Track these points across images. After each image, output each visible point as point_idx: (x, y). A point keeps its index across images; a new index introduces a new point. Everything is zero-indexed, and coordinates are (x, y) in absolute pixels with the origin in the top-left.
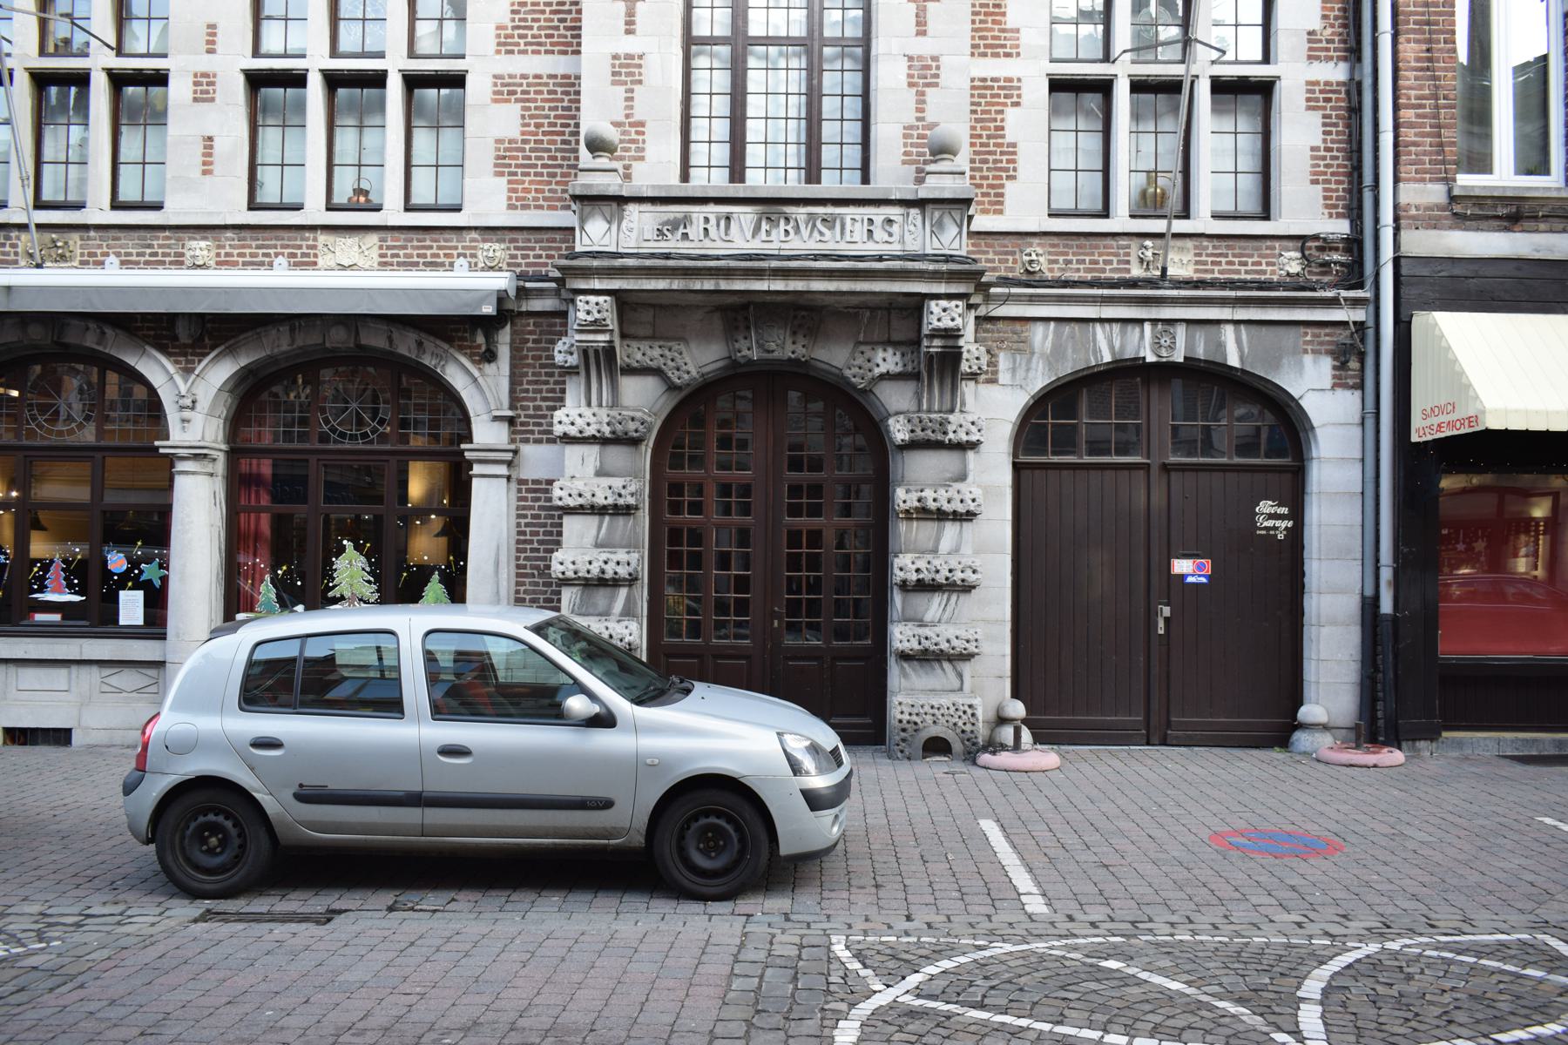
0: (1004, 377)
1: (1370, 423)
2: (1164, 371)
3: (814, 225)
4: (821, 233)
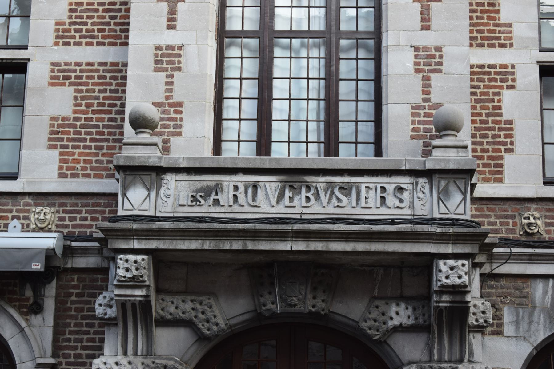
0: (508, 330)
3: (333, 193)
4: (339, 200)
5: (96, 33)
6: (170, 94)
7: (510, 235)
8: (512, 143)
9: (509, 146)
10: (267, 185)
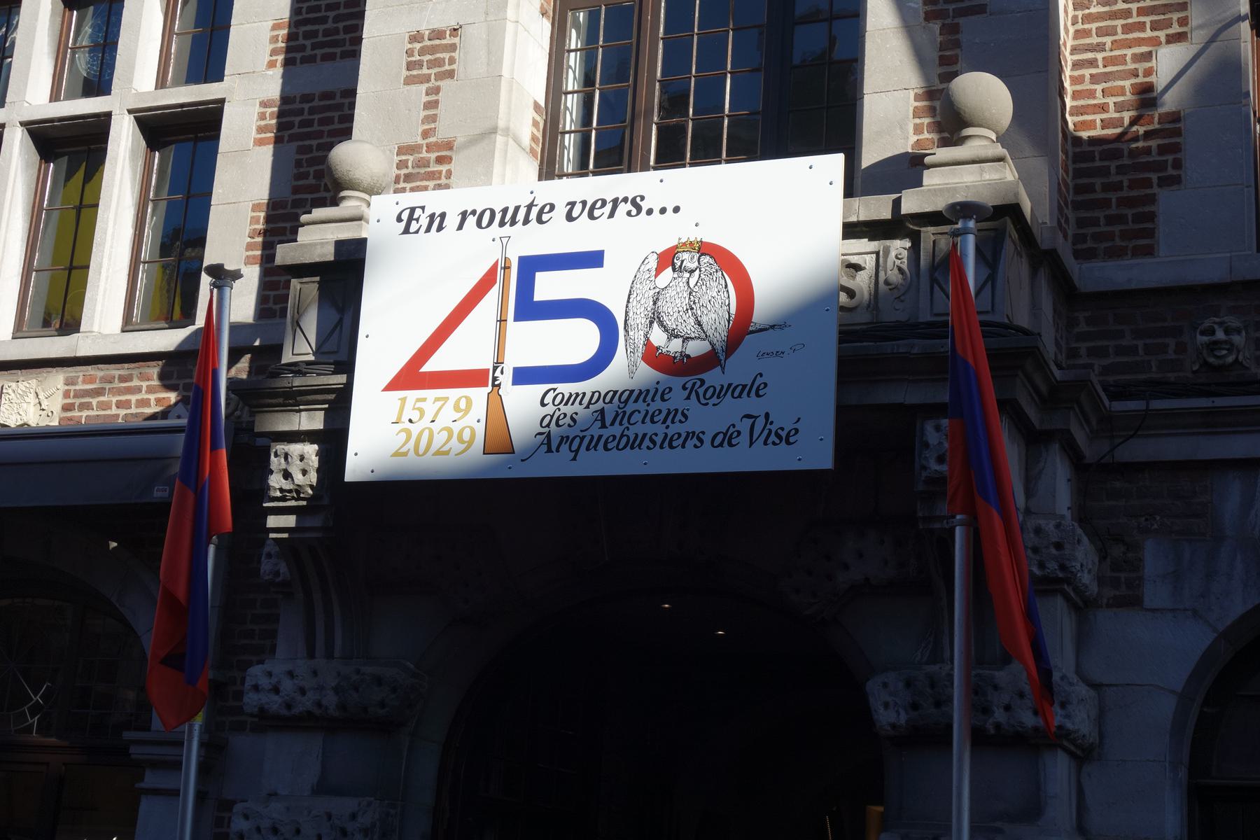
0: (1156, 593)
5: (341, 36)
6: (433, 126)
7: (1169, 375)
8: (1177, 164)
9: (1171, 171)
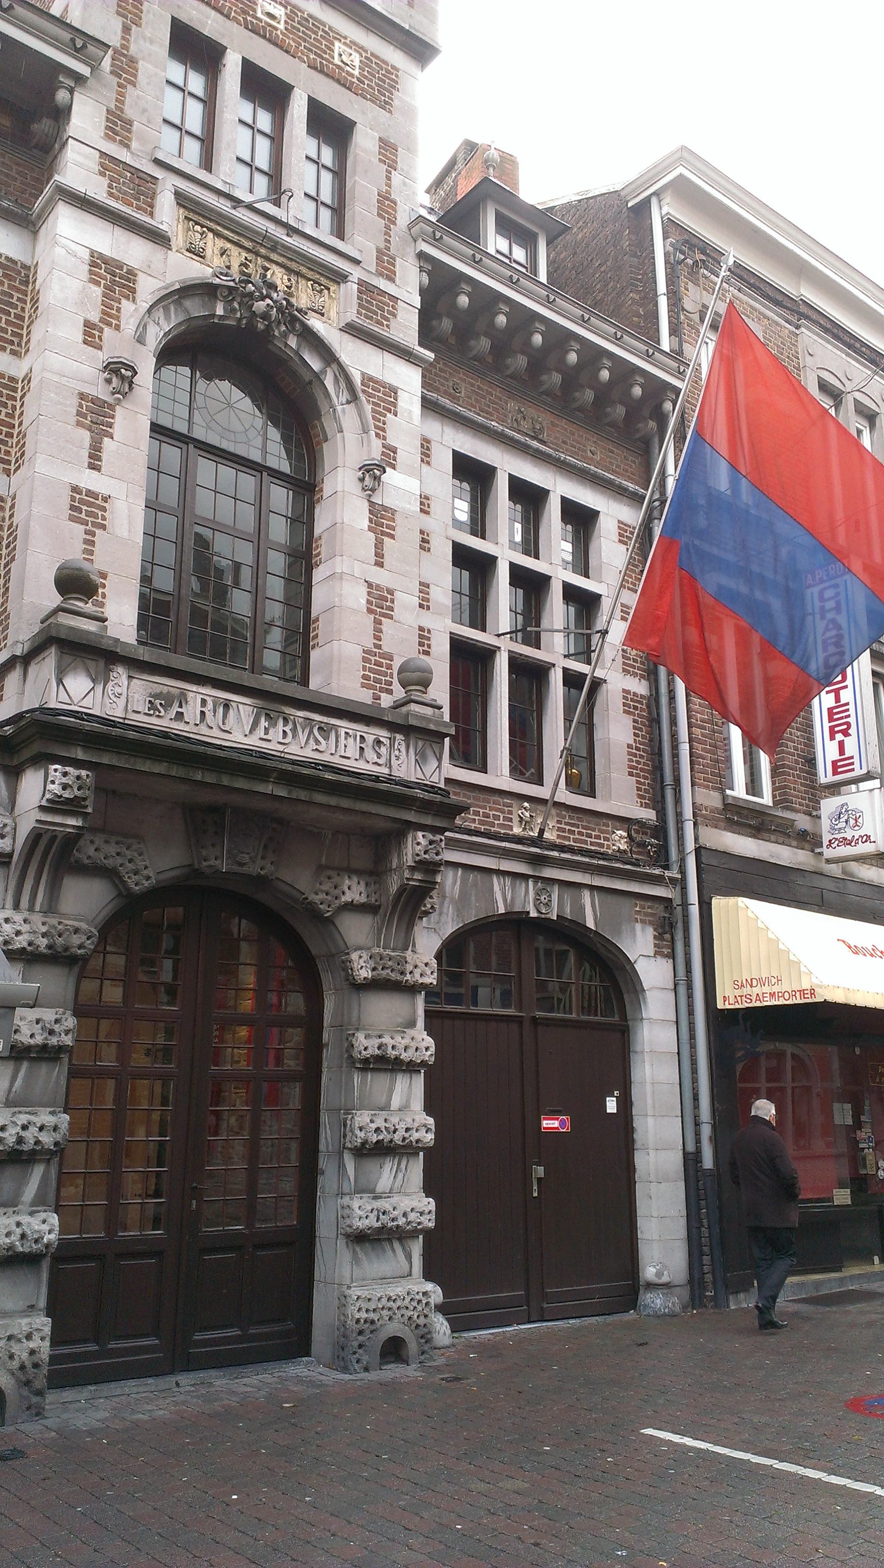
1: (682, 990)
2: (541, 925)
3: (311, 732)
4: (317, 742)
10: (241, 706)
